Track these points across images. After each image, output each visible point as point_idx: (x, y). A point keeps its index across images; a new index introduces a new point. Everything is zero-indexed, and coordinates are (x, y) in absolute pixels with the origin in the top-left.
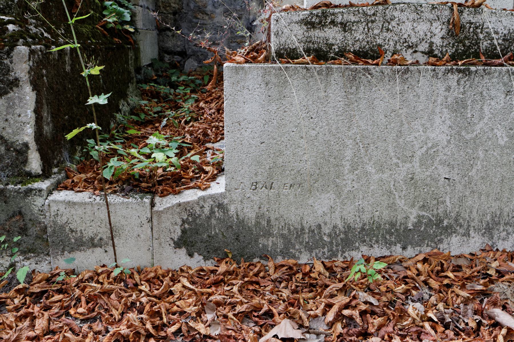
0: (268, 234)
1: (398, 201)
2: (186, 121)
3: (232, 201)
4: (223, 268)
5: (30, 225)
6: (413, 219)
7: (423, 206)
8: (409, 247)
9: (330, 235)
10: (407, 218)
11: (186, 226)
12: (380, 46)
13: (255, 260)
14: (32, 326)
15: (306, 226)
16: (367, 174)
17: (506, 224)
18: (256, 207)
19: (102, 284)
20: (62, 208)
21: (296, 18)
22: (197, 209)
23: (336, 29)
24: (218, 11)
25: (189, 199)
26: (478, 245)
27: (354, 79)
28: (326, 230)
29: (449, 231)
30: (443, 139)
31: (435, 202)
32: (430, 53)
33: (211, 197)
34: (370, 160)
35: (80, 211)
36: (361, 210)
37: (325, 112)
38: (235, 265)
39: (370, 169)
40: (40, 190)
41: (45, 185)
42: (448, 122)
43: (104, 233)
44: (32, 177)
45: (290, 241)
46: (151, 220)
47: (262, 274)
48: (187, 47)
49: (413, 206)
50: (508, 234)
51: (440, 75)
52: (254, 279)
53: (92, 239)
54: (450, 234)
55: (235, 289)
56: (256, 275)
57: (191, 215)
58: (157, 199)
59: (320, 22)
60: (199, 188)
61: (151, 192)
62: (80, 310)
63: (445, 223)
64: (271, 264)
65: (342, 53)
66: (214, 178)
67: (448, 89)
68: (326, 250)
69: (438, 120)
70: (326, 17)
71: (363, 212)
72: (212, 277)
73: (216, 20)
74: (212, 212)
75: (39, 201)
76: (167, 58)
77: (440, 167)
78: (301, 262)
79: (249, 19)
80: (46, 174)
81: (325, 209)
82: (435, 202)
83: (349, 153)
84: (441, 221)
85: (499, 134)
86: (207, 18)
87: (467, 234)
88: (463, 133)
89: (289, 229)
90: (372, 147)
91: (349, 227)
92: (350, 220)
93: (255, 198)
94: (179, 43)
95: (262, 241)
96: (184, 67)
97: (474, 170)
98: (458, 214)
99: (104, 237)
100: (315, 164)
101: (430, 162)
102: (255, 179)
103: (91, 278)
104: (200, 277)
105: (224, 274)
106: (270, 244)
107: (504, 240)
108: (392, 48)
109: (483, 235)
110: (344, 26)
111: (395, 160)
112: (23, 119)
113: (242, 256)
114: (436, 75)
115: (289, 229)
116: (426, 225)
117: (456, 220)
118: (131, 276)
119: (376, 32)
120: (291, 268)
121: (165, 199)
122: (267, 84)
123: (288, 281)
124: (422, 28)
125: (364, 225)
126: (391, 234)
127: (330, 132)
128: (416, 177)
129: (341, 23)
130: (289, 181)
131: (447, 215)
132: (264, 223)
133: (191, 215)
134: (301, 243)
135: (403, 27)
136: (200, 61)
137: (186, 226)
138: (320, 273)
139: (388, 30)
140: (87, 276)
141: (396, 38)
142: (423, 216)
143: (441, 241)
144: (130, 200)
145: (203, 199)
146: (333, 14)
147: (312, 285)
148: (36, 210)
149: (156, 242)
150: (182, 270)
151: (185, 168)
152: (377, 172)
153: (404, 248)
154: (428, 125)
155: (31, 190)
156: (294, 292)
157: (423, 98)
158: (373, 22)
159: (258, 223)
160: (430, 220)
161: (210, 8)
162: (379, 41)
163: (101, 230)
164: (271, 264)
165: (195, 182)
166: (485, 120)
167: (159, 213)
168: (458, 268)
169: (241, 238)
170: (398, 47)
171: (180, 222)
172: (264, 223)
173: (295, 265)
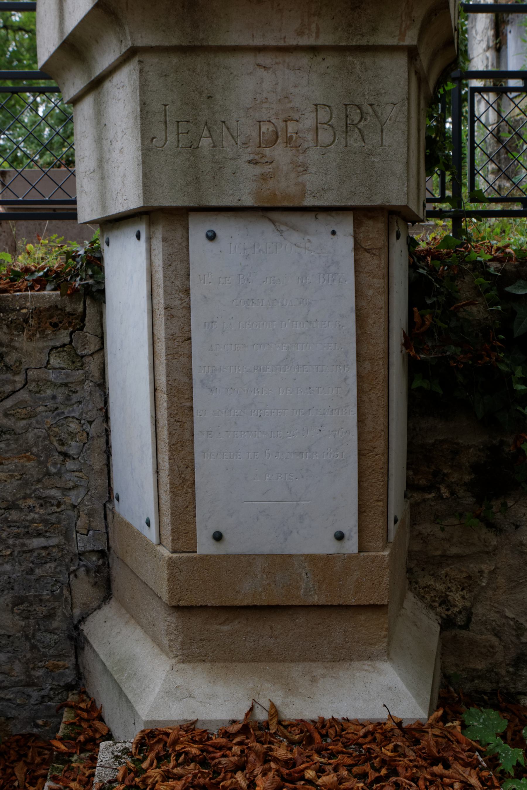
79: (72, 617)
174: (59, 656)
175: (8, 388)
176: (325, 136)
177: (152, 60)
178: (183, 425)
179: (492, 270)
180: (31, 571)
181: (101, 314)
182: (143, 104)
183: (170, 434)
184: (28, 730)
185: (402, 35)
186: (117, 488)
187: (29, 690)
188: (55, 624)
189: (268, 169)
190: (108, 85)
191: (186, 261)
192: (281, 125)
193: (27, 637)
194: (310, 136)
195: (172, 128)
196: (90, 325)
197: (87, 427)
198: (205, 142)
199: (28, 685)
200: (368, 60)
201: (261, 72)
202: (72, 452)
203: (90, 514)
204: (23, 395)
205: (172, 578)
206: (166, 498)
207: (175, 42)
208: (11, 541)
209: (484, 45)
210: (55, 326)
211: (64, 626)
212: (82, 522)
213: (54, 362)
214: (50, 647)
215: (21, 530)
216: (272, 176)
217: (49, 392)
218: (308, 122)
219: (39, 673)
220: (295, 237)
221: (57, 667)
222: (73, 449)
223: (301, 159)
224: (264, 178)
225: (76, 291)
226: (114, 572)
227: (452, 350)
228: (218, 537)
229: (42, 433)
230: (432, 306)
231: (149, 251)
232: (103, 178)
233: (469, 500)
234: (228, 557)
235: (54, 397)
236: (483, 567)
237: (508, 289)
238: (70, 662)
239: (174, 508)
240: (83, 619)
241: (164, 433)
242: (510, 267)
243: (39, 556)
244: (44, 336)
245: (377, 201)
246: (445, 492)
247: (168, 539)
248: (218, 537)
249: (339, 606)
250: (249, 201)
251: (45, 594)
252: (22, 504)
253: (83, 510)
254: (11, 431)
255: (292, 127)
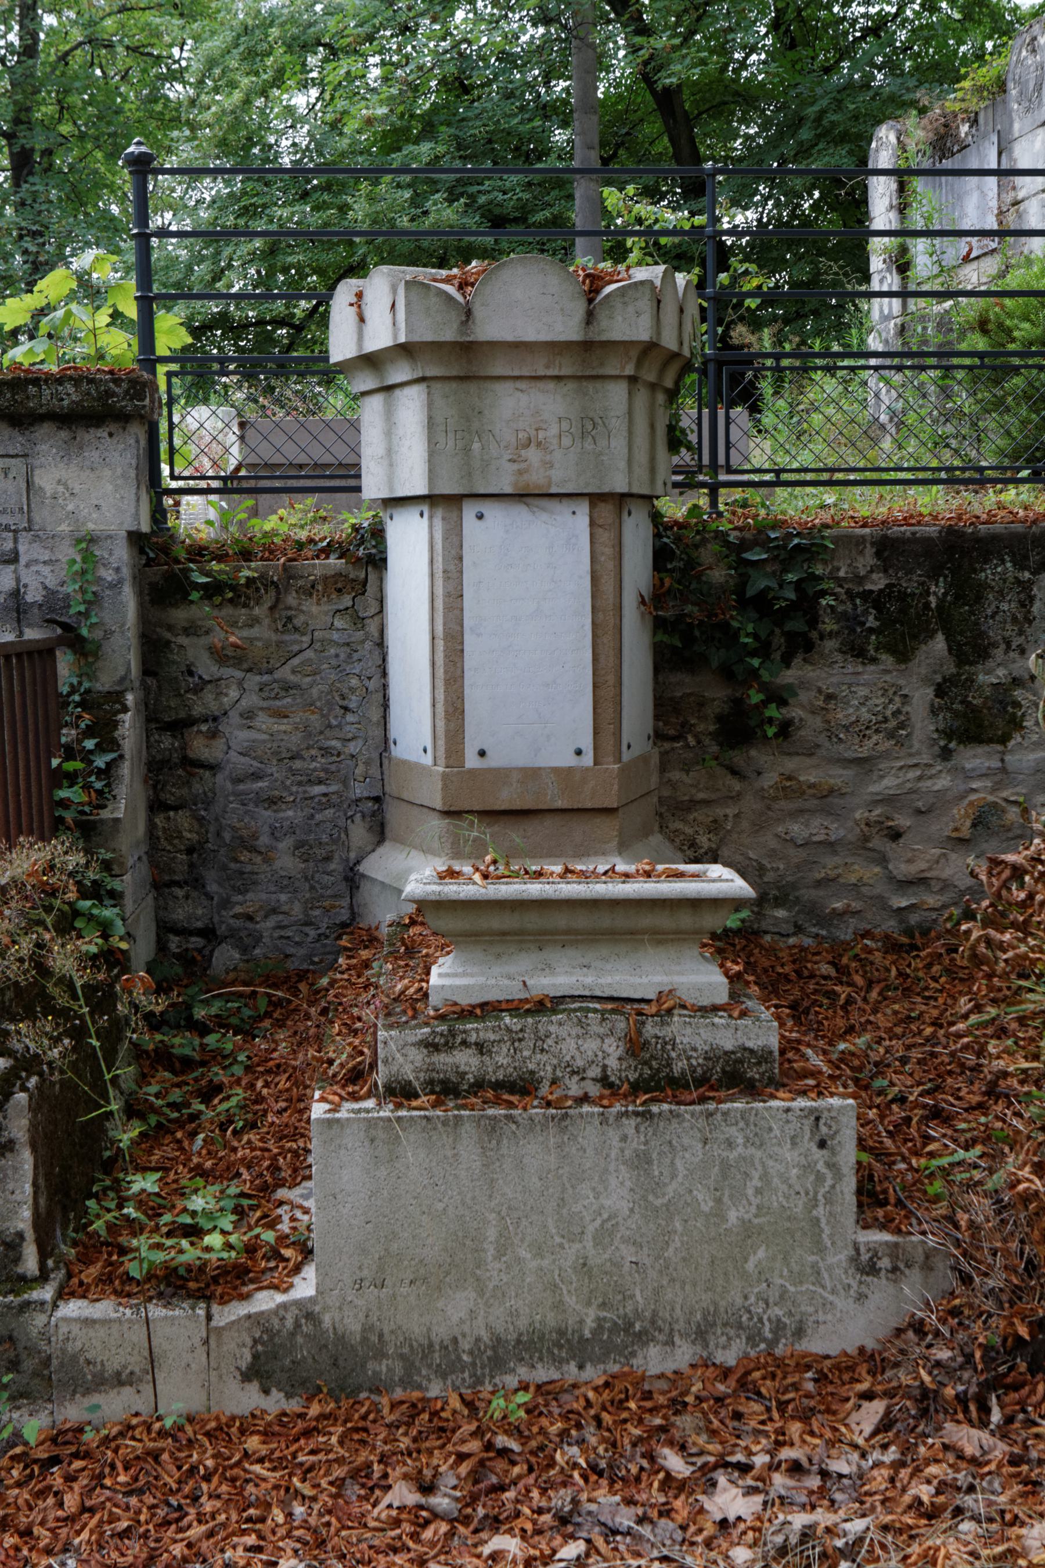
0: (380, 1354)
1: (567, 1299)
2: (235, 1132)
3: (326, 1308)
4: (314, 1410)
5: (24, 1356)
6: (590, 1323)
7: (604, 1304)
8: (588, 1366)
9: (471, 1353)
10: (581, 1322)
11: (260, 1348)
12: (532, 1073)
13: (363, 1395)
14: (60, 1505)
15: (436, 1341)
16: (519, 1260)
17: (725, 1325)
18: (361, 1316)
19: (140, 1441)
20: (75, 1329)
21: (412, 1039)
22: (276, 1322)
23: (469, 1051)
24: (281, 846)
25: (264, 1307)
26: (687, 1357)
27: (493, 1127)
28: (466, 1345)
29: (643, 1338)
30: (624, 1206)
31: (620, 1297)
32: (604, 1080)
33: (298, 1303)
34: (522, 1240)
35: (102, 1332)
36: (513, 1314)
37: (456, 1176)
38: (332, 1405)
39: (524, 1253)
40: (43, 1303)
41: (46, 1293)
42: (628, 1184)
43: (136, 1363)
44: (25, 1282)
45: (413, 1364)
46: (206, 1342)
47: (371, 1417)
48: (216, 919)
49: (589, 1304)
50: (729, 1339)
51: (611, 1120)
52: (362, 1424)
53: (118, 1374)
54: (646, 1344)
55: (334, 1440)
56: (364, 1418)
57: (266, 1331)
58: (215, 1308)
59: (447, 1043)
60: (276, 1288)
61: (204, 1296)
62: (122, 1479)
63: (638, 1327)
64: (385, 1401)
65: (479, 1085)
66: (297, 1269)
67: (624, 1138)
68: (466, 1375)
69: (613, 1182)
70: (454, 1036)
71: (518, 1316)
72: (300, 1425)
73: (278, 864)
74: (297, 1325)
75: (40, 1319)
76: (174, 943)
77: (622, 1247)
78: (432, 1394)
79: (347, 860)
80: (43, 1277)
81: (462, 1314)
82: (620, 1297)
83: (492, 1233)
84: (631, 1325)
85: (700, 1197)
86: (259, 859)
87: (670, 1343)
88: (651, 1198)
89: (411, 1346)
90: (524, 1222)
91: (499, 1340)
92: (500, 1327)
93: (360, 1302)
94: (200, 912)
95: (371, 1366)
96: (210, 960)
97: (671, 1250)
98: (655, 1313)
99: (137, 1370)
100: (445, 1250)
101: (607, 1240)
102: (359, 1275)
103: (121, 1434)
104: (283, 1425)
105: (317, 1419)
106: (384, 1369)
107: (724, 1348)
108: (549, 1075)
109: (693, 1343)
110: (481, 1048)
111: (558, 1240)
112: (18, 1197)
113: (342, 1390)
114: (604, 1120)
115: (411, 1346)
116: (610, 1331)
117: (653, 1322)
118: (181, 1429)
119: (526, 1053)
120: (414, 1405)
121: (226, 1309)
122: (372, 1141)
123: (408, 1425)
124: (591, 1046)
125: (521, 1335)
126: (561, 1347)
127: (463, 1203)
128: (590, 1262)
129: (476, 1044)
130: (409, 1275)
131: (638, 1315)
132: (375, 1339)
133: (266, 1331)
134: (430, 1366)
135: (563, 1046)
136: (244, 950)
137: (260, 1348)
138: (454, 1412)
139: (542, 1050)
140: (115, 1430)
141: (555, 1062)
142: (605, 1319)
143: (633, 1354)
144: (177, 1312)
145: (284, 1306)
146: (465, 1032)
147: (442, 1430)
148: (34, 1333)
149: (213, 1373)
150: (253, 1416)
151: (251, 1249)
152: (534, 1257)
153: (581, 1367)
154: (600, 1188)
155: (28, 1303)
156: (415, 1440)
157: (590, 1152)
158: (520, 1040)
159: (365, 1339)
160: (615, 1324)
161: (264, 840)
162: (531, 1066)
163: (132, 1360)
164: (385, 1401)
165: (268, 1275)
166: (680, 1179)
167: (219, 1330)
168: (648, 1395)
169: (341, 1363)
170: (559, 1074)
171: (249, 1342)
172: (375, 1339)
173: (422, 1399)
174: (335, 896)
175: (296, 648)
176: (566, 441)
177: (437, 386)
178: (455, 663)
179: (731, 539)
180: (312, 817)
181: (381, 580)
182: (430, 418)
183: (446, 672)
184: (305, 966)
185: (623, 368)
186: (393, 734)
187: (307, 929)
188: (332, 866)
189: (523, 466)
190: (397, 392)
191: (460, 535)
192: (533, 433)
193: (306, 879)
194: (555, 441)
195: (451, 435)
196: (371, 589)
197: (366, 682)
198: (476, 446)
199: (307, 924)
200: (598, 385)
201: (519, 394)
202: (352, 705)
203: (367, 763)
204: (309, 654)
205: (445, 787)
206: (441, 724)
207: (454, 373)
208: (294, 789)
209: (886, 202)
210: (339, 591)
211: (340, 868)
212: (360, 770)
213: (338, 623)
214: (327, 888)
215: (304, 778)
216: (526, 471)
217: (333, 651)
218: (554, 430)
219: (317, 912)
220: (544, 516)
221: (333, 907)
222: (353, 703)
223: (548, 458)
224: (520, 472)
225: (359, 559)
226: (388, 816)
227: (688, 609)
228: (482, 753)
229: (325, 688)
230: (672, 571)
231: (431, 527)
232: (391, 465)
233: (715, 749)
234: (489, 770)
235: (337, 656)
236: (728, 811)
237: (745, 555)
238: (345, 902)
239: (447, 732)
240: (358, 862)
241: (440, 672)
242: (748, 535)
243: (320, 803)
244: (329, 601)
245: (606, 489)
246: (691, 740)
247: (442, 761)
248: (482, 753)
249: (579, 810)
250: (508, 490)
251: (325, 838)
252: (306, 754)
253: (362, 759)
254: (297, 687)
255: (541, 435)
